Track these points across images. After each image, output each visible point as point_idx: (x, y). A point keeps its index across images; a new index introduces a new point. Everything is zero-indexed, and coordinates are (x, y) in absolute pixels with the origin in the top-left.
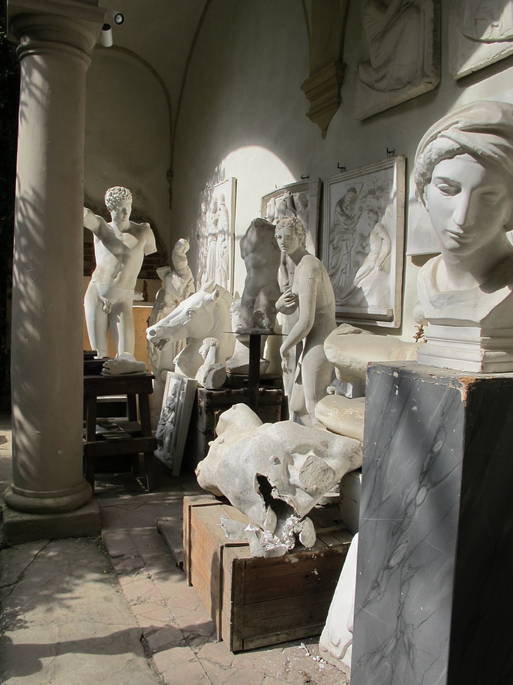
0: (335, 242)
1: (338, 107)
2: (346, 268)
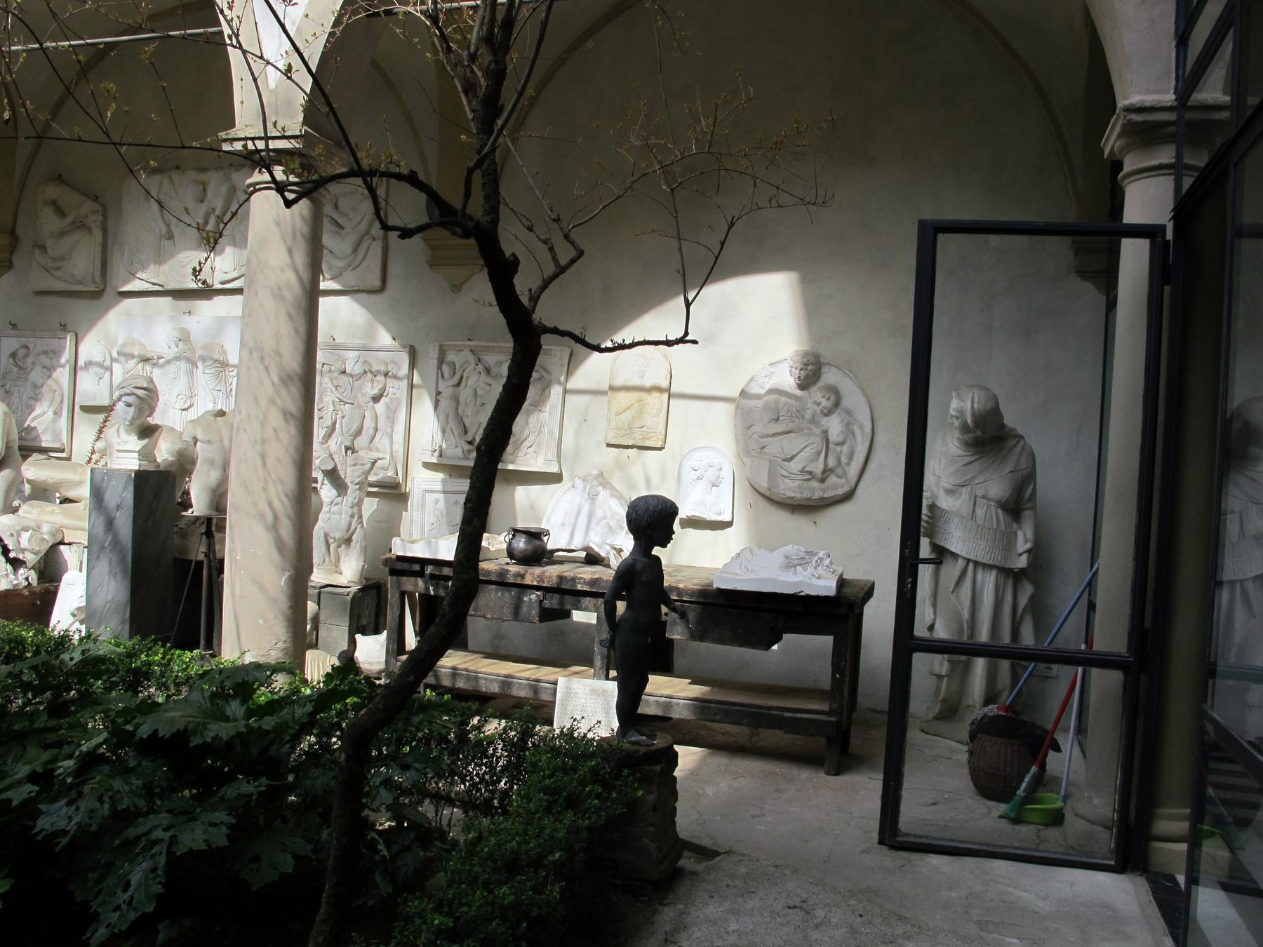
0: (7, 387)
1: (9, 270)
2: (17, 409)
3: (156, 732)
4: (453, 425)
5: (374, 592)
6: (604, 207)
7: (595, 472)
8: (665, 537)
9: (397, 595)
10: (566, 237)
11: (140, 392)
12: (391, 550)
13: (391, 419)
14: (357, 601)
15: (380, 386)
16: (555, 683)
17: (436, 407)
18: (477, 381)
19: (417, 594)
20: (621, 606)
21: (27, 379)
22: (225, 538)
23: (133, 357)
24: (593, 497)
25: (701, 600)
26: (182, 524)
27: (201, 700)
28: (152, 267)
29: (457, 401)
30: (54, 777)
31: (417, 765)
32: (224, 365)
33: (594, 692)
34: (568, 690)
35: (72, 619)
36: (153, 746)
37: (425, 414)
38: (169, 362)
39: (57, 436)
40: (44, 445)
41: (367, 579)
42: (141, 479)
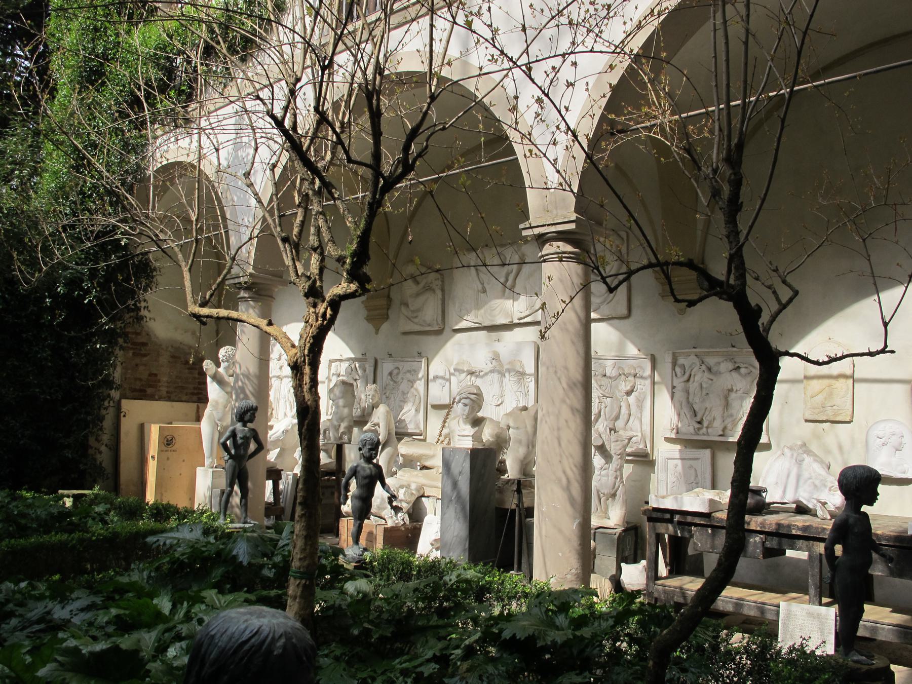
3: (514, 635)
4: (685, 410)
5: (633, 532)
6: (808, 256)
7: (799, 443)
8: (872, 498)
9: (654, 536)
10: (784, 282)
11: (473, 397)
12: (647, 503)
13: (640, 407)
14: (621, 539)
15: (631, 384)
16: (778, 606)
17: (672, 398)
18: (702, 377)
19: (666, 536)
20: (838, 549)
21: (398, 389)
22: (533, 493)
23: (464, 372)
24: (799, 462)
25: (897, 544)
26: (499, 484)
27: (539, 613)
28: (473, 312)
29: (688, 393)
30: (449, 660)
31: (693, 670)
32: (522, 374)
33: (810, 614)
34: (789, 614)
35: (431, 547)
36: (511, 645)
37: (664, 400)
38: (486, 374)
39: (418, 426)
40: (410, 431)
41: (627, 523)
42: (475, 454)
